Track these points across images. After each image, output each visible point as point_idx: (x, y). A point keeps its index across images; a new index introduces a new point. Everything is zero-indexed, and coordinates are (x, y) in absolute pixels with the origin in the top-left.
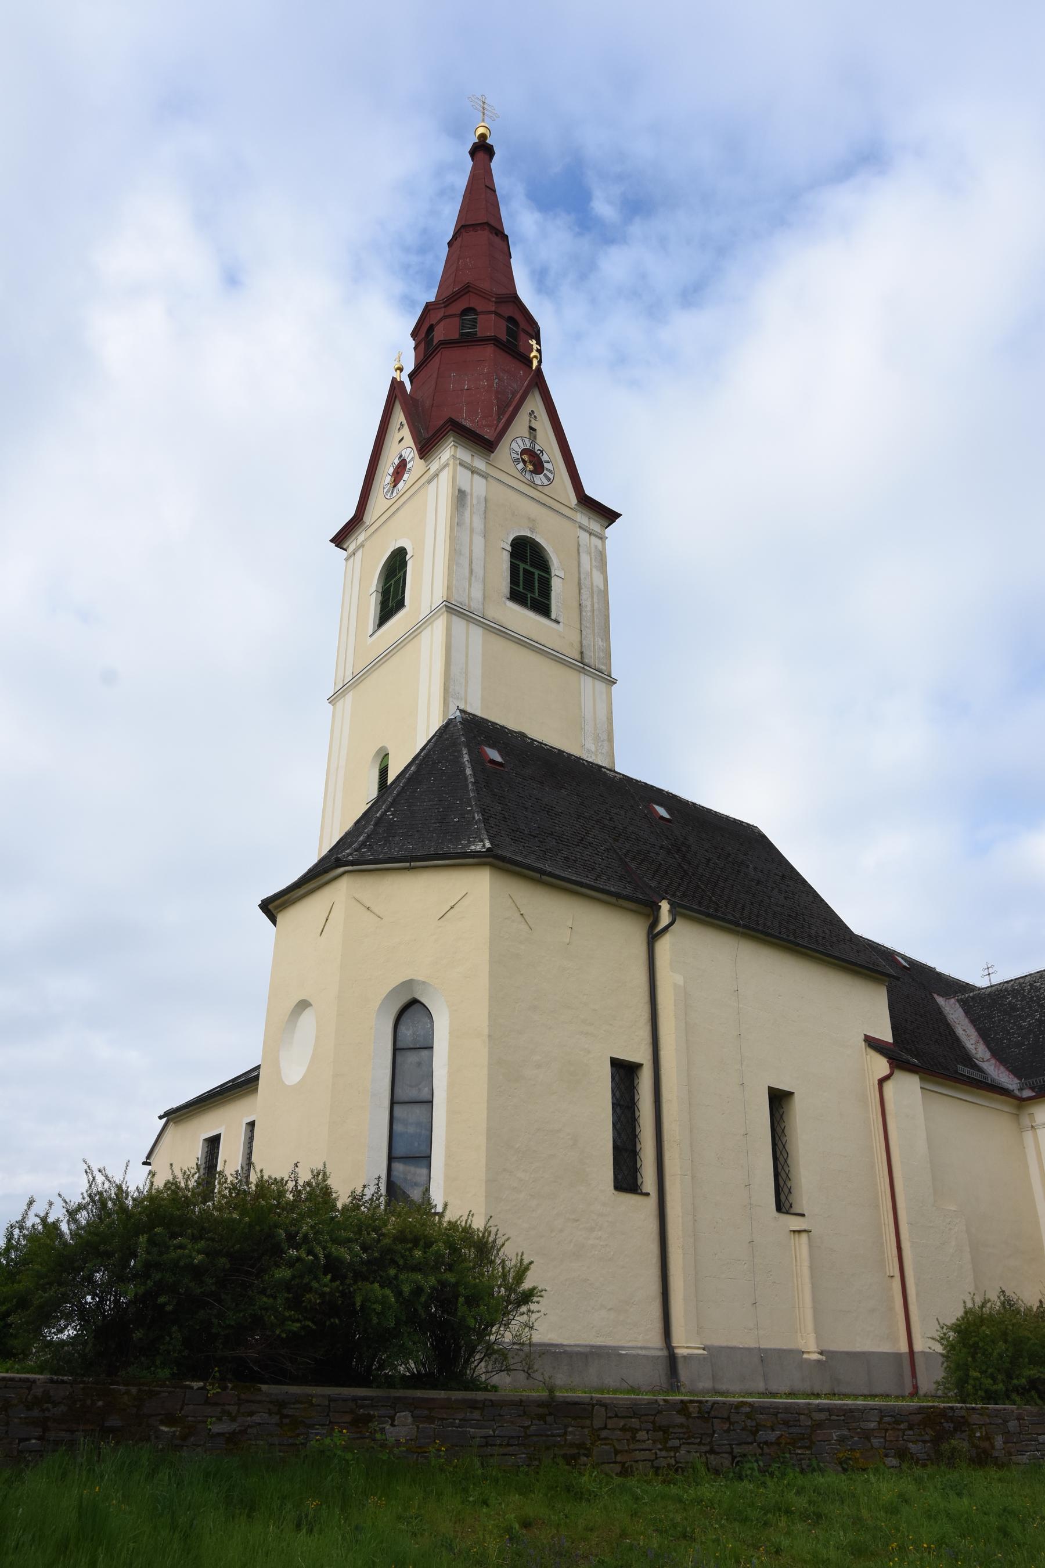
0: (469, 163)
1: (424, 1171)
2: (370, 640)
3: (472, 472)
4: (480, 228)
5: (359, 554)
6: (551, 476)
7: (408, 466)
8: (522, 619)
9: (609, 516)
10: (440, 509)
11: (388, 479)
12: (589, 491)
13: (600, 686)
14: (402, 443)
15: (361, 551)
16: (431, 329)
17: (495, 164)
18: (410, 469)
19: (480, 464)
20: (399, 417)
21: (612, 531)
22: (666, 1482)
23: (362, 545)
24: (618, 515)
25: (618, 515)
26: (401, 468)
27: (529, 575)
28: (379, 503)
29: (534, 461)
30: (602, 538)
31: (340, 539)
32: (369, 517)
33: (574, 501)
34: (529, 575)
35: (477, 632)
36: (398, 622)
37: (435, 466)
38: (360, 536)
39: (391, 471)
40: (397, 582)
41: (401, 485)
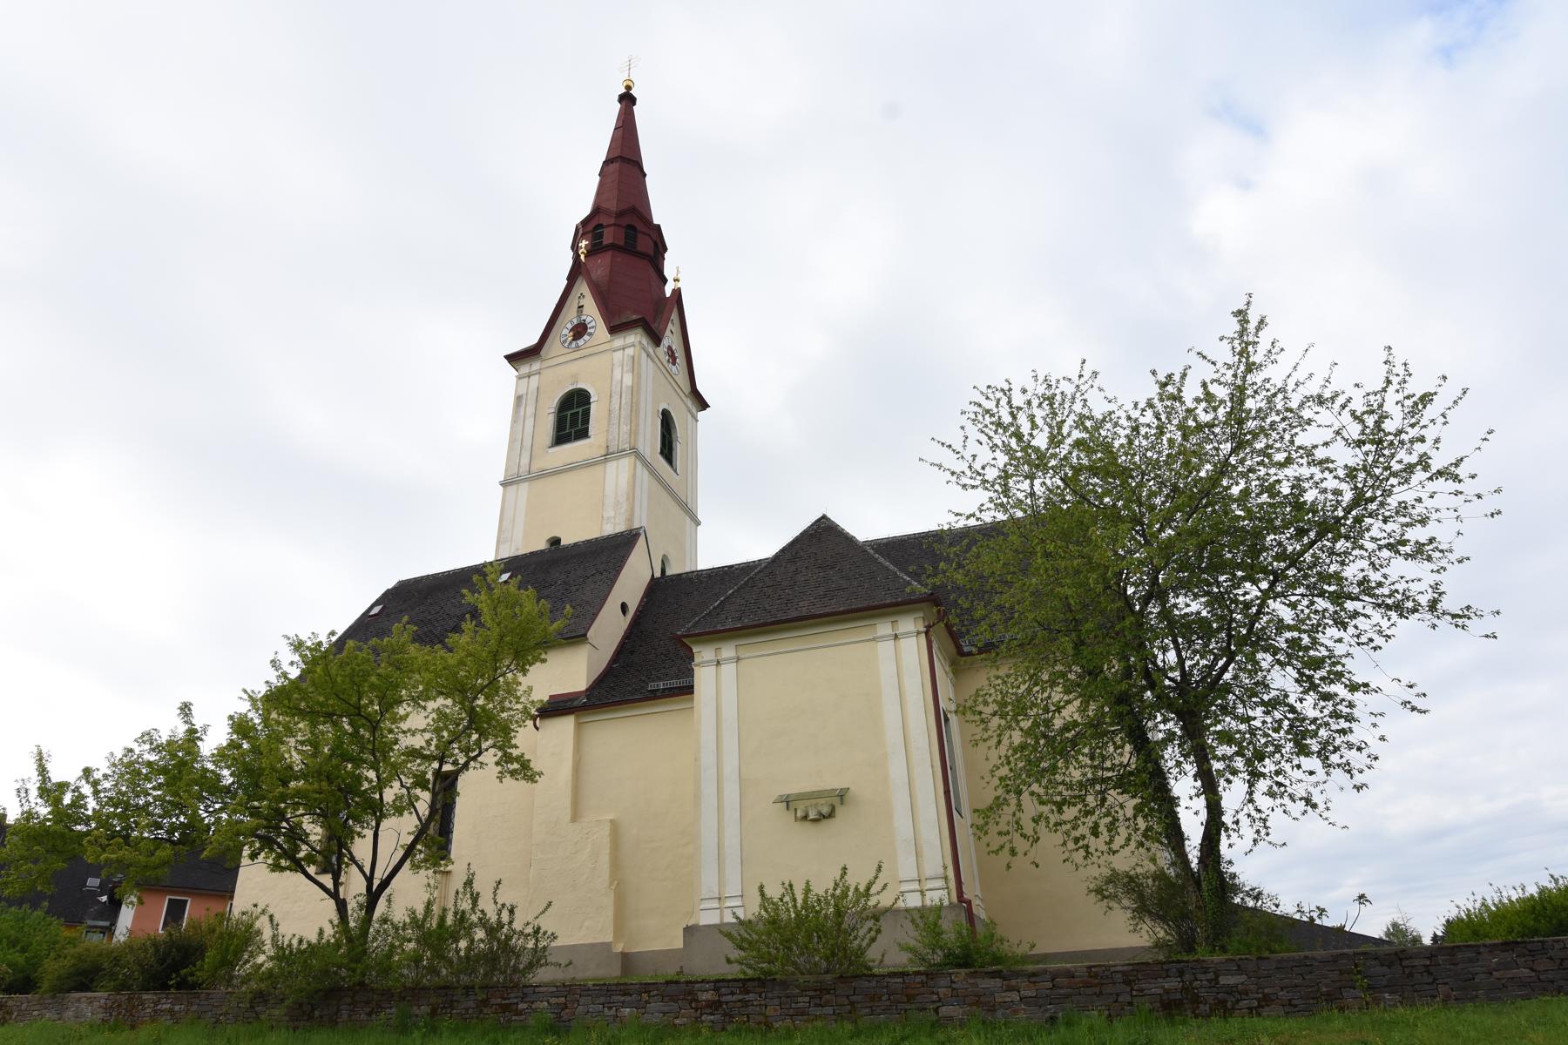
9: (703, 405)
10: (613, 366)
20: (583, 288)
21: (701, 415)
26: (580, 330)
28: (554, 347)
31: (514, 358)
33: (687, 389)
35: (646, 473)
36: (574, 450)
41: (581, 342)
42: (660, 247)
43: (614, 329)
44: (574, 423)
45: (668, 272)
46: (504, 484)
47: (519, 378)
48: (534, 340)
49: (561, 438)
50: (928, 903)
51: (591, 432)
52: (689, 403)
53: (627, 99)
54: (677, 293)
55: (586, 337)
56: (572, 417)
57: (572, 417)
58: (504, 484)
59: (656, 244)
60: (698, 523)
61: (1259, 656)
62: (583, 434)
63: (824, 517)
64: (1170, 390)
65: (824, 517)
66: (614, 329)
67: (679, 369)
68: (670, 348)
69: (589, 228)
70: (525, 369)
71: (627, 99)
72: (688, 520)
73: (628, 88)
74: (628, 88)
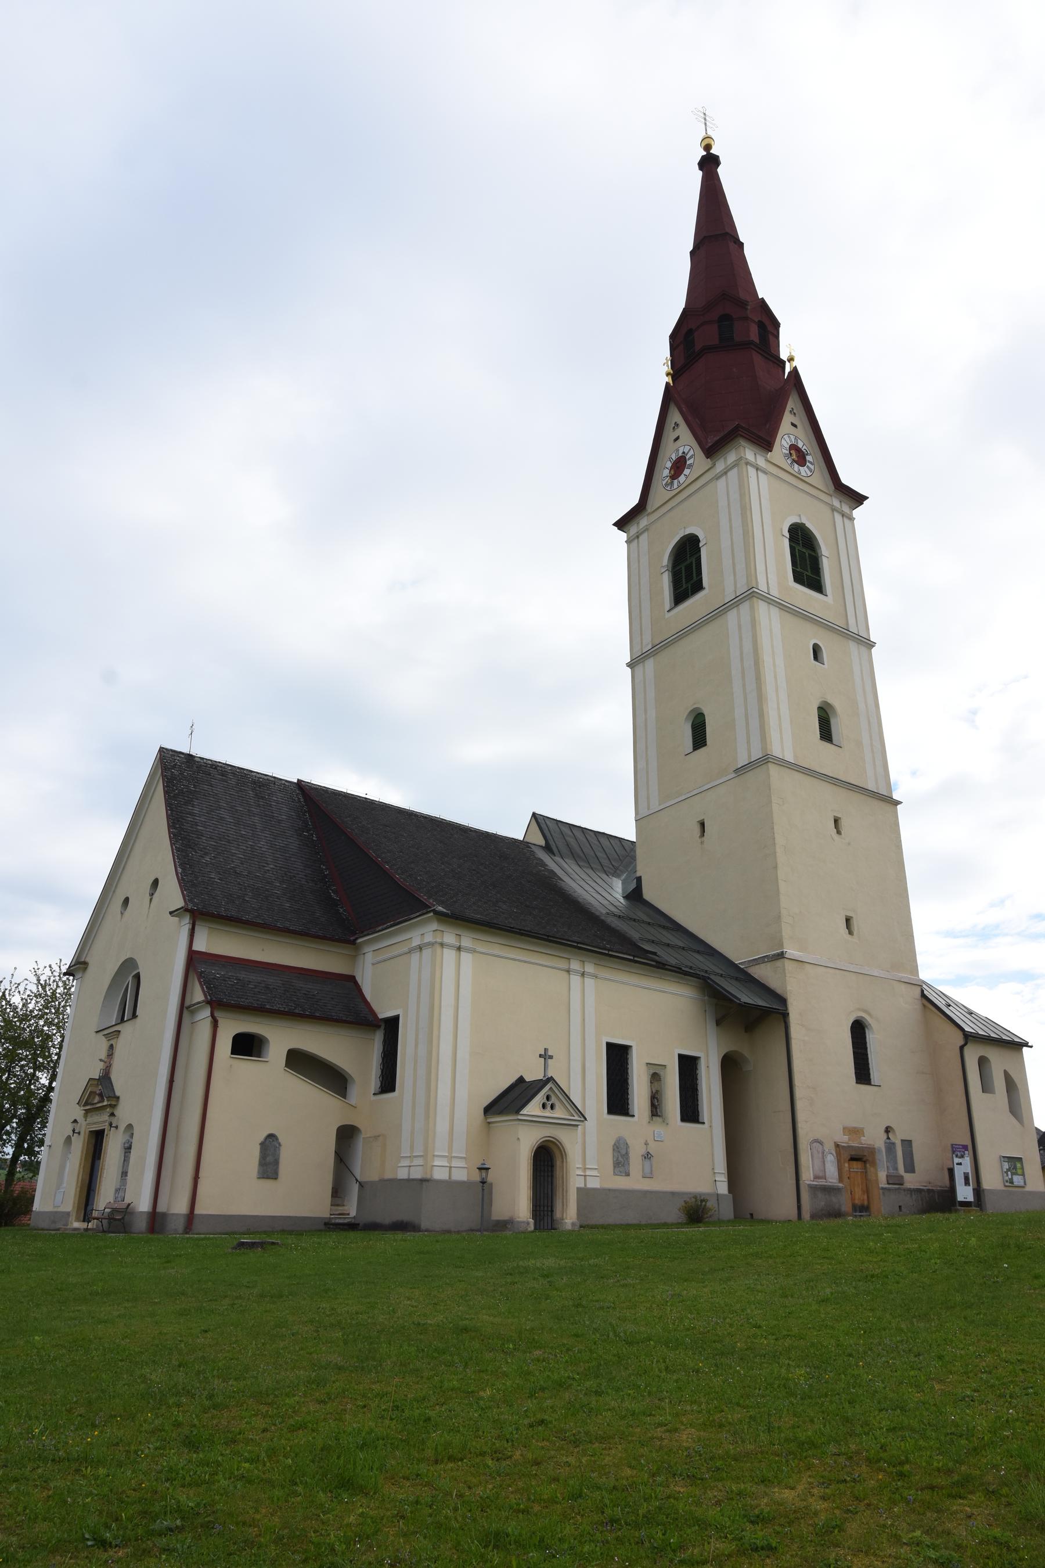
2: (668, 615)
3: (757, 469)
4: (716, 240)
5: (644, 538)
6: (812, 467)
7: (688, 462)
8: (802, 595)
9: (859, 499)
11: (666, 472)
12: (845, 480)
14: (684, 442)
15: (646, 534)
16: (690, 332)
17: (720, 170)
18: (691, 466)
19: (761, 462)
20: (675, 416)
21: (857, 513)
22: (41, 1143)
23: (646, 529)
24: (866, 498)
25: (866, 498)
26: (679, 466)
27: (806, 560)
29: (799, 456)
30: (851, 519)
31: (621, 524)
32: (650, 508)
33: (827, 485)
34: (806, 560)
35: (775, 611)
36: (695, 604)
37: (720, 466)
38: (643, 521)
39: (669, 465)
40: (689, 568)
41: (682, 478)
43: (711, 451)
44: (689, 577)
45: (784, 355)
46: (629, 665)
47: (629, 542)
48: (634, 500)
50: (589, 1186)
52: (836, 503)
53: (709, 163)
54: (795, 372)
55: (687, 471)
59: (761, 325)
60: (871, 645)
62: (698, 587)
63: (162, 750)
64: (668, 374)
65: (162, 750)
66: (711, 451)
68: (794, 447)
69: (684, 340)
70: (634, 529)
71: (709, 163)
72: (852, 646)
73: (708, 148)
74: (708, 148)
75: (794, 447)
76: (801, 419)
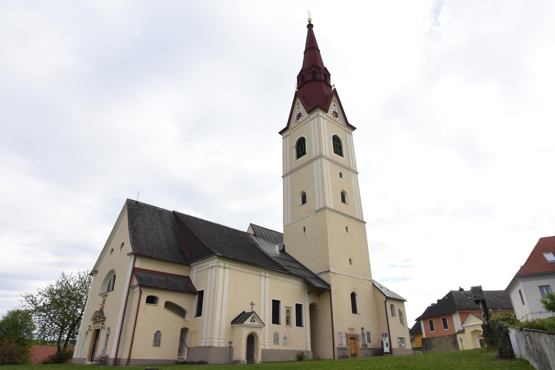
0: (307, 29)
1: (135, 266)
5: (288, 137)
8: (337, 157)
9: (354, 128)
11: (295, 118)
12: (350, 123)
13: (355, 174)
14: (301, 108)
16: (303, 76)
17: (313, 29)
20: (298, 101)
21: (353, 133)
22: (77, 334)
26: (299, 116)
28: (293, 124)
29: (336, 115)
30: (352, 134)
31: (281, 133)
32: (290, 128)
35: (328, 162)
37: (312, 116)
38: (288, 132)
41: (300, 120)
42: (327, 75)
43: (309, 112)
44: (302, 150)
45: (332, 84)
46: (282, 177)
49: (299, 156)
51: (307, 152)
52: (347, 129)
53: (310, 26)
54: (335, 90)
56: (301, 148)
57: (301, 148)
58: (282, 177)
59: (325, 75)
60: (357, 173)
61: (78, 309)
62: (304, 153)
63: (128, 200)
65: (128, 200)
66: (309, 112)
67: (340, 120)
68: (334, 112)
69: (301, 78)
70: (285, 135)
71: (310, 26)
72: (352, 173)
73: (310, 22)
74: (310, 22)
75: (334, 112)
76: (336, 104)
